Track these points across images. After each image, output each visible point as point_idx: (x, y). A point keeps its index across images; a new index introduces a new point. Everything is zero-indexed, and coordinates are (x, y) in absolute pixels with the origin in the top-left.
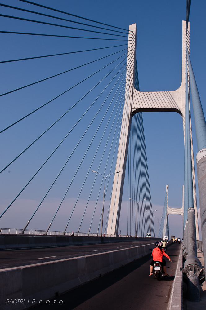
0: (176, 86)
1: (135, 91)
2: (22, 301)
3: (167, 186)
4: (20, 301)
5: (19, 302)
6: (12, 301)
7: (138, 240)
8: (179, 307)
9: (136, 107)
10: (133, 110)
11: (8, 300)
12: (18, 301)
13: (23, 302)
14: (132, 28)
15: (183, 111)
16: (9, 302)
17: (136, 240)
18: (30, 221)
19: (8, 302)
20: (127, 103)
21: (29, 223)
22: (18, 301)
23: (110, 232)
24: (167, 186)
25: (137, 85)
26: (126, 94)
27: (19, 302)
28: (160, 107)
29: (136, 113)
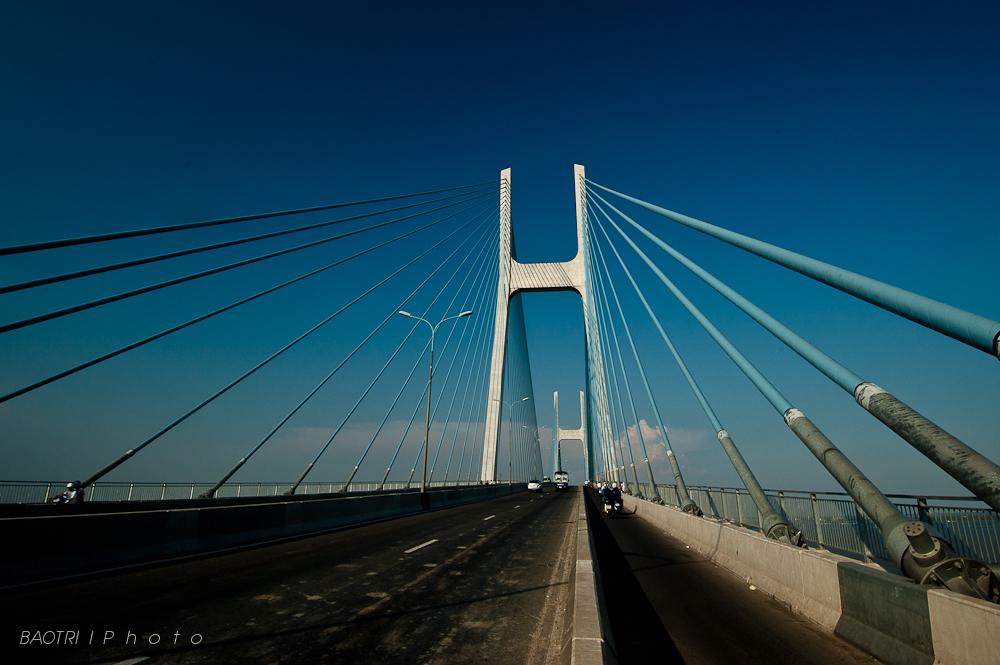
0: (569, 254)
1: (514, 262)
2: (70, 635)
3: (556, 393)
4: (63, 635)
5: (62, 640)
6: (37, 637)
7: (914, 502)
8: (902, 526)
9: (515, 286)
10: (512, 290)
11: (26, 634)
12: (57, 634)
13: (74, 640)
14: (506, 174)
15: (583, 291)
16: (31, 639)
17: (930, 502)
18: (135, 451)
19: (25, 640)
20: (503, 281)
21: (242, 464)
22: (57, 634)
23: (487, 476)
24: (556, 393)
25: (514, 255)
26: (501, 266)
27: (62, 640)
28: (545, 286)
29: (516, 295)
